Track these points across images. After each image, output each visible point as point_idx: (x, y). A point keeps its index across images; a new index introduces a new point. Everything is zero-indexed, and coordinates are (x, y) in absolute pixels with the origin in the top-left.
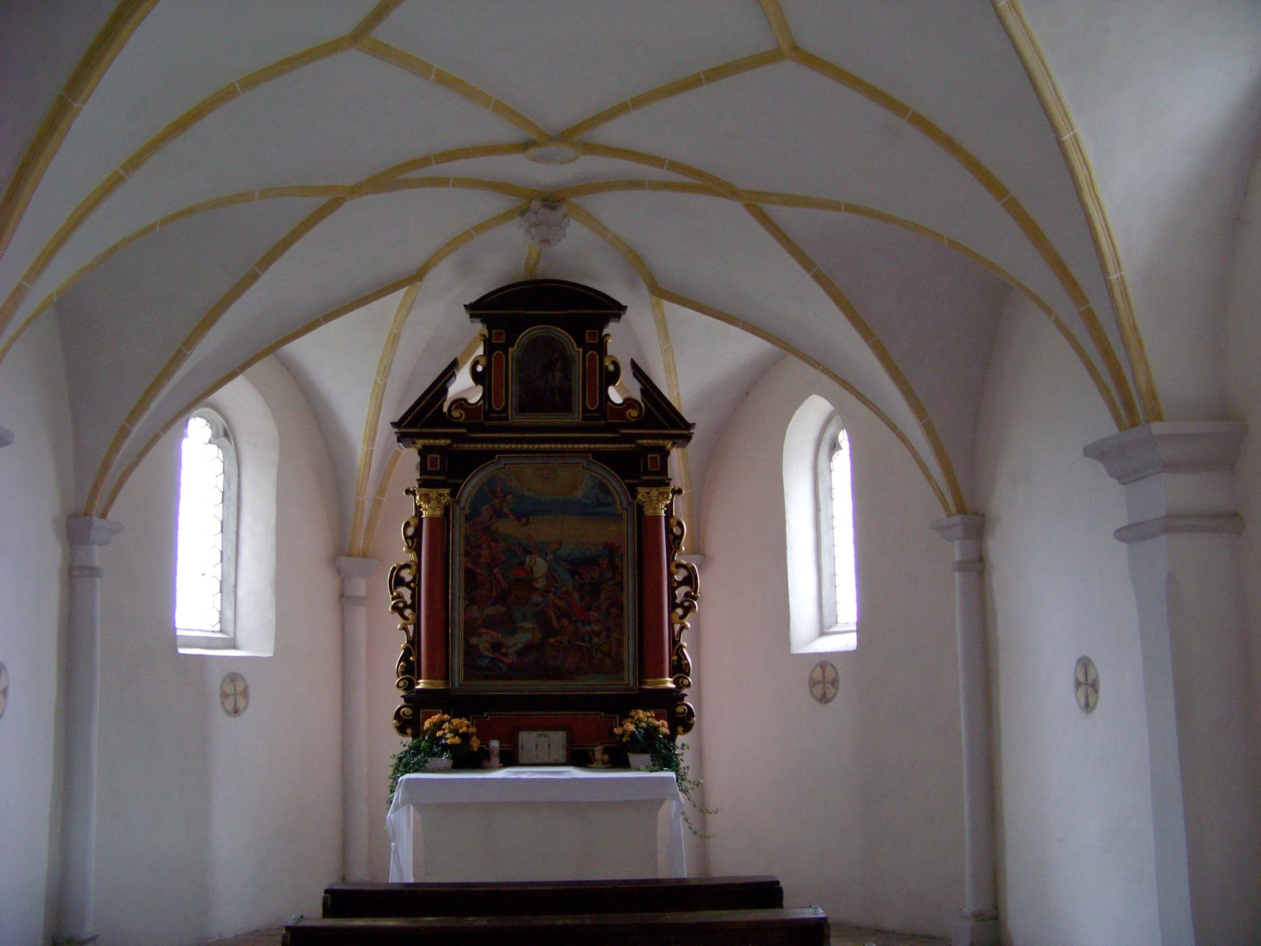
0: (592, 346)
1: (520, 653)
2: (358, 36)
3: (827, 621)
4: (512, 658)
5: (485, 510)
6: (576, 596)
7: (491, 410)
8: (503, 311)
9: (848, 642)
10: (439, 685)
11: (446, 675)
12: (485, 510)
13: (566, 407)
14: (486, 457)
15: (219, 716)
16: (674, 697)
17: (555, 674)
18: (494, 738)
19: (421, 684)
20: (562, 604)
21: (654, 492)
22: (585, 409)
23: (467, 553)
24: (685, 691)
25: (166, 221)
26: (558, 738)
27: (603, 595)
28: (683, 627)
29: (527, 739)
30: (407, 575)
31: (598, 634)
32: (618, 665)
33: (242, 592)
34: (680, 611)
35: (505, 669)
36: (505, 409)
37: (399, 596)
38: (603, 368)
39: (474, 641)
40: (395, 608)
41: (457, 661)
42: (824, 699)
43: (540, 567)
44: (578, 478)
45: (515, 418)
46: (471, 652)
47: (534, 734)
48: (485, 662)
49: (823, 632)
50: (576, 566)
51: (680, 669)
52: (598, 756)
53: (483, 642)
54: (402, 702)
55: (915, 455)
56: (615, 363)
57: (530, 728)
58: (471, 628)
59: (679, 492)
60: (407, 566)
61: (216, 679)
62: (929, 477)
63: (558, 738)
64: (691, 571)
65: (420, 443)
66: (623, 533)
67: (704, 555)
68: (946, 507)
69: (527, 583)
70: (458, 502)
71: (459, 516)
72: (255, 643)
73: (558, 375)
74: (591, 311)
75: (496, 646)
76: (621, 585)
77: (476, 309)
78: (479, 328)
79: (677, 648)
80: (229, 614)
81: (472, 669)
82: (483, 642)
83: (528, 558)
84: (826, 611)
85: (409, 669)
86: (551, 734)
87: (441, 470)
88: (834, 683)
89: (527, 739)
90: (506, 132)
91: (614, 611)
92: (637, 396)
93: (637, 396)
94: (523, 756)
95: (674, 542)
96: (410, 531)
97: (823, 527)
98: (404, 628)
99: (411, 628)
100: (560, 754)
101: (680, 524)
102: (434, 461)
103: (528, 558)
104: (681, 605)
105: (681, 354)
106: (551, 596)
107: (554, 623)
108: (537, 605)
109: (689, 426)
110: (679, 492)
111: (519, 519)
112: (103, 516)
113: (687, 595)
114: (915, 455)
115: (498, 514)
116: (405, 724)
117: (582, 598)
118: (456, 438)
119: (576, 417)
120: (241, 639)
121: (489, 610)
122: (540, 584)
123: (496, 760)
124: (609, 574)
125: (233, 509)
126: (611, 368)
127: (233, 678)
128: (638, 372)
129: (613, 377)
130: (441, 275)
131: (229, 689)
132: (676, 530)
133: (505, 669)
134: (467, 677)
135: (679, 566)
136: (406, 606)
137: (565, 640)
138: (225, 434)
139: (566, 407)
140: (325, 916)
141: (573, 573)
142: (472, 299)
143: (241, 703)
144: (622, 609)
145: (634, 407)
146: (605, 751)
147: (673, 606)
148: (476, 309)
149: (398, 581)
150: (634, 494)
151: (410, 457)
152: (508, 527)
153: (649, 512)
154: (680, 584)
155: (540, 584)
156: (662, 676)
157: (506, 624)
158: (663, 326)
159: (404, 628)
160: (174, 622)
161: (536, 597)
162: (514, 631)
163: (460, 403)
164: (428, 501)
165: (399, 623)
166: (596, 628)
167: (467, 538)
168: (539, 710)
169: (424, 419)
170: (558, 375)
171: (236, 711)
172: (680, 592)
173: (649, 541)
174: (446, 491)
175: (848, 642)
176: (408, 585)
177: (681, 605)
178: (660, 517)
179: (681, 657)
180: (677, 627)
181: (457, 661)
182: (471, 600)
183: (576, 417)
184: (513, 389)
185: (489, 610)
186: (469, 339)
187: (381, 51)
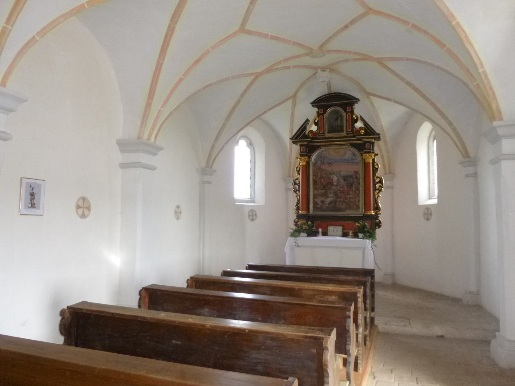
0: (349, 112)
1: (329, 204)
2: (242, 30)
3: (431, 195)
4: (327, 205)
5: (319, 163)
6: (346, 187)
7: (320, 133)
8: (322, 103)
9: (435, 201)
10: (304, 212)
11: (307, 209)
12: (319, 163)
13: (343, 131)
14: (319, 147)
15: (247, 220)
16: (376, 217)
17: (340, 210)
18: (320, 228)
19: (300, 212)
20: (342, 189)
21: (368, 155)
22: (347, 131)
23: (314, 175)
24: (379, 215)
25: (204, 88)
26: (340, 228)
27: (354, 186)
28: (378, 196)
29: (331, 228)
30: (297, 182)
31: (352, 198)
32: (358, 207)
33: (256, 187)
34: (377, 191)
35: (325, 208)
36: (324, 133)
37: (295, 188)
38: (353, 118)
39: (316, 200)
40: (294, 191)
41: (311, 206)
42: (428, 219)
43: (335, 178)
44: (349, 152)
45: (327, 135)
46: (315, 203)
47: (333, 227)
48: (319, 206)
49: (430, 198)
50: (345, 178)
51: (377, 208)
52: (351, 234)
53: (319, 201)
54: (296, 217)
55: (452, 138)
56: (357, 116)
57: (332, 225)
58: (315, 196)
59: (377, 155)
60: (297, 179)
61: (247, 211)
62: (457, 146)
63: (340, 228)
64: (381, 179)
65: (299, 143)
66: (359, 168)
67: (394, 174)
68: (463, 155)
69: (331, 183)
70: (311, 160)
71: (311, 164)
72: (260, 200)
73: (339, 121)
74: (346, 101)
75: (322, 202)
76: (359, 183)
77: (314, 104)
78: (316, 109)
79: (376, 202)
80: (253, 194)
81: (315, 208)
82: (319, 201)
83: (331, 176)
84: (431, 192)
85: (298, 208)
86: (338, 227)
87: (307, 151)
88: (431, 214)
89: (331, 228)
90: (302, 51)
91: (357, 191)
92: (363, 126)
93: (363, 126)
94: (329, 233)
95: (375, 170)
96: (298, 169)
97: (431, 164)
98: (296, 197)
99: (298, 197)
100: (340, 233)
101: (377, 165)
102: (303, 149)
103: (331, 176)
104: (378, 189)
105: (380, 113)
106: (338, 187)
107: (339, 195)
108: (334, 189)
109: (378, 134)
110: (377, 155)
111: (329, 164)
112: (212, 168)
113: (380, 186)
114: (452, 138)
115: (323, 163)
116: (296, 223)
117: (347, 187)
118: (309, 142)
119: (345, 133)
120: (256, 200)
121: (320, 191)
122: (335, 183)
123: (320, 234)
124: (355, 180)
125: (253, 165)
126: (355, 118)
127: (252, 211)
128: (362, 119)
129: (356, 121)
130: (301, 94)
131: (251, 214)
132: (376, 167)
133: (325, 208)
134: (314, 211)
135: (377, 177)
136: (297, 190)
137: (342, 200)
138: (250, 144)
139: (343, 131)
140: (222, 275)
141: (345, 180)
142: (311, 102)
143: (254, 218)
144: (359, 191)
145: (362, 129)
146: (352, 233)
147: (375, 189)
148: (314, 104)
149: (295, 184)
150: (362, 155)
151: (296, 148)
152: (325, 167)
153: (367, 161)
154: (378, 183)
155: (335, 183)
156: (370, 210)
157: (325, 195)
158: (372, 104)
159: (296, 197)
160: (233, 196)
161: (334, 187)
162: (328, 197)
163: (311, 132)
164: (301, 160)
165: (295, 195)
166: (351, 196)
167: (314, 171)
168: (335, 220)
169: (299, 136)
170: (339, 121)
171: (253, 220)
172: (378, 186)
173: (369, 170)
174: (307, 157)
175: (435, 201)
176: (297, 184)
177: (378, 189)
178: (370, 163)
179: (378, 205)
180: (376, 196)
181: (311, 206)
182: (315, 189)
183: (345, 133)
184: (326, 126)
185: (320, 191)
186: (312, 113)
187: (249, 32)
